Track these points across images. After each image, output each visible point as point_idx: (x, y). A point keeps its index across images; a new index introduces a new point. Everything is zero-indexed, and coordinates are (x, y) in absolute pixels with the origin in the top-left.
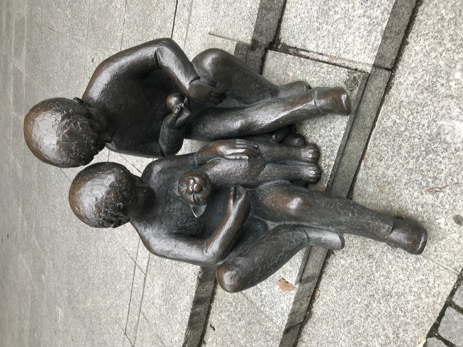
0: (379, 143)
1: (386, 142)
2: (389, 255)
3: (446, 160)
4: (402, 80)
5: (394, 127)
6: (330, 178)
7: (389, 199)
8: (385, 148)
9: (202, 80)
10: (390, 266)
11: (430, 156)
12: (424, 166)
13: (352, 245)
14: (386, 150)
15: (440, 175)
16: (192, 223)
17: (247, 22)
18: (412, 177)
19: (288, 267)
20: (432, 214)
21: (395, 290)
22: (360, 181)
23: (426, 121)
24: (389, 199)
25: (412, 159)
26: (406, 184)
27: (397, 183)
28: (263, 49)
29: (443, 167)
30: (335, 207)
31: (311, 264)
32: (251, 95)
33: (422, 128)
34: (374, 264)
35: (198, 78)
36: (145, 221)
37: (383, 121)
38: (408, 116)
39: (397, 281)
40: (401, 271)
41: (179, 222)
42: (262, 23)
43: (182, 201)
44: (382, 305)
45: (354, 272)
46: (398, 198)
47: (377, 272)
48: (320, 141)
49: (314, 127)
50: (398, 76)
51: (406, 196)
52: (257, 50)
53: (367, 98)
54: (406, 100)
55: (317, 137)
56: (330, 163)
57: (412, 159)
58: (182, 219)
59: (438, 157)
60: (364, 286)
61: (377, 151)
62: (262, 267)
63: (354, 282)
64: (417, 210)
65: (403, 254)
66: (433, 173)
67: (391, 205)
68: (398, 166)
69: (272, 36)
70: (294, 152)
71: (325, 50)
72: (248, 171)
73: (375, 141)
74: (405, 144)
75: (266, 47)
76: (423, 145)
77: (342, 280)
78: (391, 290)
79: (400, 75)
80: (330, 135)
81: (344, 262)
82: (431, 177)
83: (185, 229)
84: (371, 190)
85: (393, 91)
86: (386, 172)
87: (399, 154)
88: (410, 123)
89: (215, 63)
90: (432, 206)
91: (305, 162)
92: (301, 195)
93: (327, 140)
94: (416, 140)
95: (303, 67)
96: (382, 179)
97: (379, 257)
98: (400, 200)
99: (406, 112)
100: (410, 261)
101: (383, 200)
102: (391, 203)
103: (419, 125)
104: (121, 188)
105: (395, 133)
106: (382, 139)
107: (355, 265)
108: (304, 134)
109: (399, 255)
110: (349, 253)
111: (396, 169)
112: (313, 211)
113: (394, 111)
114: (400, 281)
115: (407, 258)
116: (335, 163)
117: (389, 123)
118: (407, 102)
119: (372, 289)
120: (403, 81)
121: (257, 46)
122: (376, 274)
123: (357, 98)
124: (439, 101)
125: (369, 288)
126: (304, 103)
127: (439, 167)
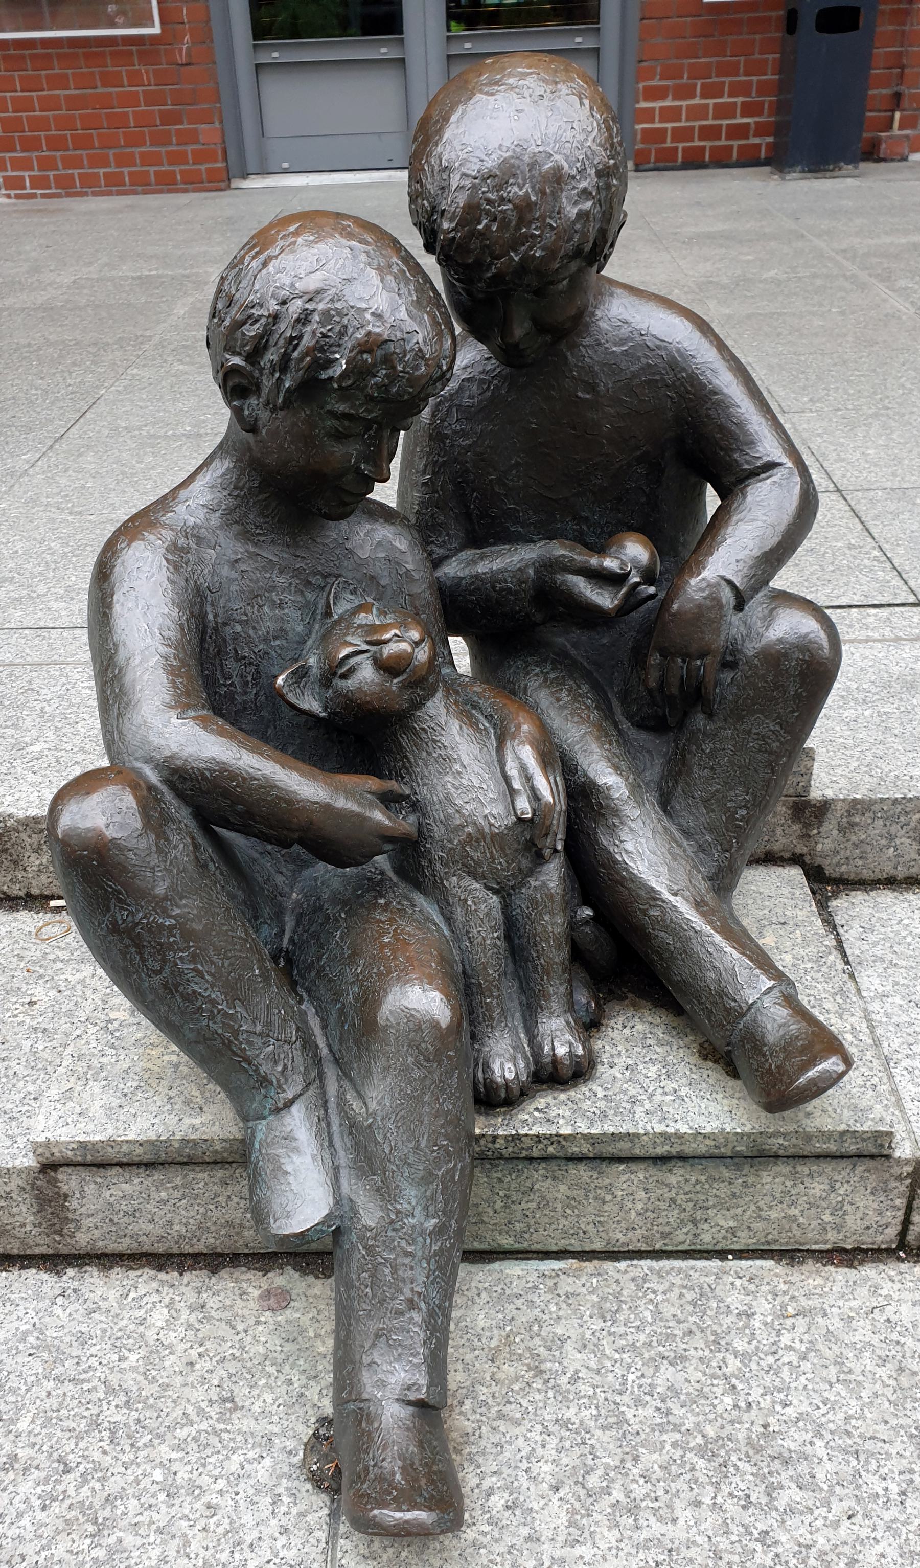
0: (654, 1292)
1: (668, 1311)
2: (267, 1462)
3: (711, 1521)
4: (887, 1288)
5: (731, 1318)
6: (505, 1137)
7: (479, 1387)
8: (647, 1314)
9: (736, 619)
10: (221, 1484)
11: (701, 1463)
12: (655, 1456)
13: (240, 1327)
14: (643, 1321)
15: (653, 1520)
16: (237, 681)
17: (867, 778)
18: (599, 1433)
19: (98, 1104)
20: (501, 1548)
21: (130, 1540)
22: (496, 1276)
23: (805, 1408)
24: (479, 1387)
25: (658, 1409)
26: (565, 1424)
27: (551, 1394)
28: (801, 849)
29: (685, 1515)
30: (448, 1153)
31: (125, 1188)
32: (705, 801)
33: (774, 1402)
34: (204, 1426)
35: (740, 605)
36: (232, 502)
37: (731, 1279)
38: (789, 1348)
39: (174, 1529)
40: (221, 1530)
41: (238, 628)
42: (881, 822)
43: (309, 635)
44: (40, 1516)
45: (134, 1369)
46: (501, 1416)
47: (178, 1448)
48: (615, 1071)
49: (649, 1042)
50: (893, 1273)
51: (521, 1440)
52: (796, 827)
53: (807, 1181)
54: (835, 1324)
55: (621, 1061)
56: (561, 1121)
57: (658, 1409)
58: (249, 642)
59: (710, 1489)
60: (95, 1424)
61: (625, 1293)
62: (171, 928)
63: (95, 1382)
64: (490, 1493)
65: (294, 1511)
66: (647, 1495)
67: (461, 1403)
68: (610, 1377)
69: (844, 868)
70: (556, 988)
71: (884, 1020)
72: (480, 831)
73: (654, 1278)
74: (695, 1369)
75: (807, 859)
76: (722, 1427)
77: (83, 1340)
78: (121, 1524)
79: (896, 1279)
80: (652, 1095)
81: (160, 1324)
82: (628, 1493)
83: (219, 653)
84: (482, 1322)
85: (841, 1275)
86: (569, 1347)
87: (655, 1363)
88: (771, 1359)
89: (804, 646)
90: (529, 1539)
91: (531, 1042)
92: (459, 1025)
93: (632, 1092)
94: (728, 1400)
95: (809, 965)
96: (537, 1341)
97: (239, 1431)
98: (495, 1424)
99: (797, 1336)
100: (279, 1544)
101: (466, 1369)
102: (468, 1402)
103: (780, 1390)
104: (401, 360)
105: (715, 1327)
106: (674, 1296)
107: (167, 1364)
108: (612, 1023)
109: (286, 1500)
110: (205, 1329)
111: (598, 1372)
112: (417, 1073)
113: (779, 1300)
114: (175, 1544)
115: (285, 1531)
116: (566, 1137)
117: (735, 1300)
118: (831, 1328)
119: (97, 1455)
120: (884, 1292)
121: (807, 826)
122: (164, 1448)
123: (808, 1138)
124: (886, 1422)
125: (94, 1446)
126: (751, 961)
127: (678, 1504)
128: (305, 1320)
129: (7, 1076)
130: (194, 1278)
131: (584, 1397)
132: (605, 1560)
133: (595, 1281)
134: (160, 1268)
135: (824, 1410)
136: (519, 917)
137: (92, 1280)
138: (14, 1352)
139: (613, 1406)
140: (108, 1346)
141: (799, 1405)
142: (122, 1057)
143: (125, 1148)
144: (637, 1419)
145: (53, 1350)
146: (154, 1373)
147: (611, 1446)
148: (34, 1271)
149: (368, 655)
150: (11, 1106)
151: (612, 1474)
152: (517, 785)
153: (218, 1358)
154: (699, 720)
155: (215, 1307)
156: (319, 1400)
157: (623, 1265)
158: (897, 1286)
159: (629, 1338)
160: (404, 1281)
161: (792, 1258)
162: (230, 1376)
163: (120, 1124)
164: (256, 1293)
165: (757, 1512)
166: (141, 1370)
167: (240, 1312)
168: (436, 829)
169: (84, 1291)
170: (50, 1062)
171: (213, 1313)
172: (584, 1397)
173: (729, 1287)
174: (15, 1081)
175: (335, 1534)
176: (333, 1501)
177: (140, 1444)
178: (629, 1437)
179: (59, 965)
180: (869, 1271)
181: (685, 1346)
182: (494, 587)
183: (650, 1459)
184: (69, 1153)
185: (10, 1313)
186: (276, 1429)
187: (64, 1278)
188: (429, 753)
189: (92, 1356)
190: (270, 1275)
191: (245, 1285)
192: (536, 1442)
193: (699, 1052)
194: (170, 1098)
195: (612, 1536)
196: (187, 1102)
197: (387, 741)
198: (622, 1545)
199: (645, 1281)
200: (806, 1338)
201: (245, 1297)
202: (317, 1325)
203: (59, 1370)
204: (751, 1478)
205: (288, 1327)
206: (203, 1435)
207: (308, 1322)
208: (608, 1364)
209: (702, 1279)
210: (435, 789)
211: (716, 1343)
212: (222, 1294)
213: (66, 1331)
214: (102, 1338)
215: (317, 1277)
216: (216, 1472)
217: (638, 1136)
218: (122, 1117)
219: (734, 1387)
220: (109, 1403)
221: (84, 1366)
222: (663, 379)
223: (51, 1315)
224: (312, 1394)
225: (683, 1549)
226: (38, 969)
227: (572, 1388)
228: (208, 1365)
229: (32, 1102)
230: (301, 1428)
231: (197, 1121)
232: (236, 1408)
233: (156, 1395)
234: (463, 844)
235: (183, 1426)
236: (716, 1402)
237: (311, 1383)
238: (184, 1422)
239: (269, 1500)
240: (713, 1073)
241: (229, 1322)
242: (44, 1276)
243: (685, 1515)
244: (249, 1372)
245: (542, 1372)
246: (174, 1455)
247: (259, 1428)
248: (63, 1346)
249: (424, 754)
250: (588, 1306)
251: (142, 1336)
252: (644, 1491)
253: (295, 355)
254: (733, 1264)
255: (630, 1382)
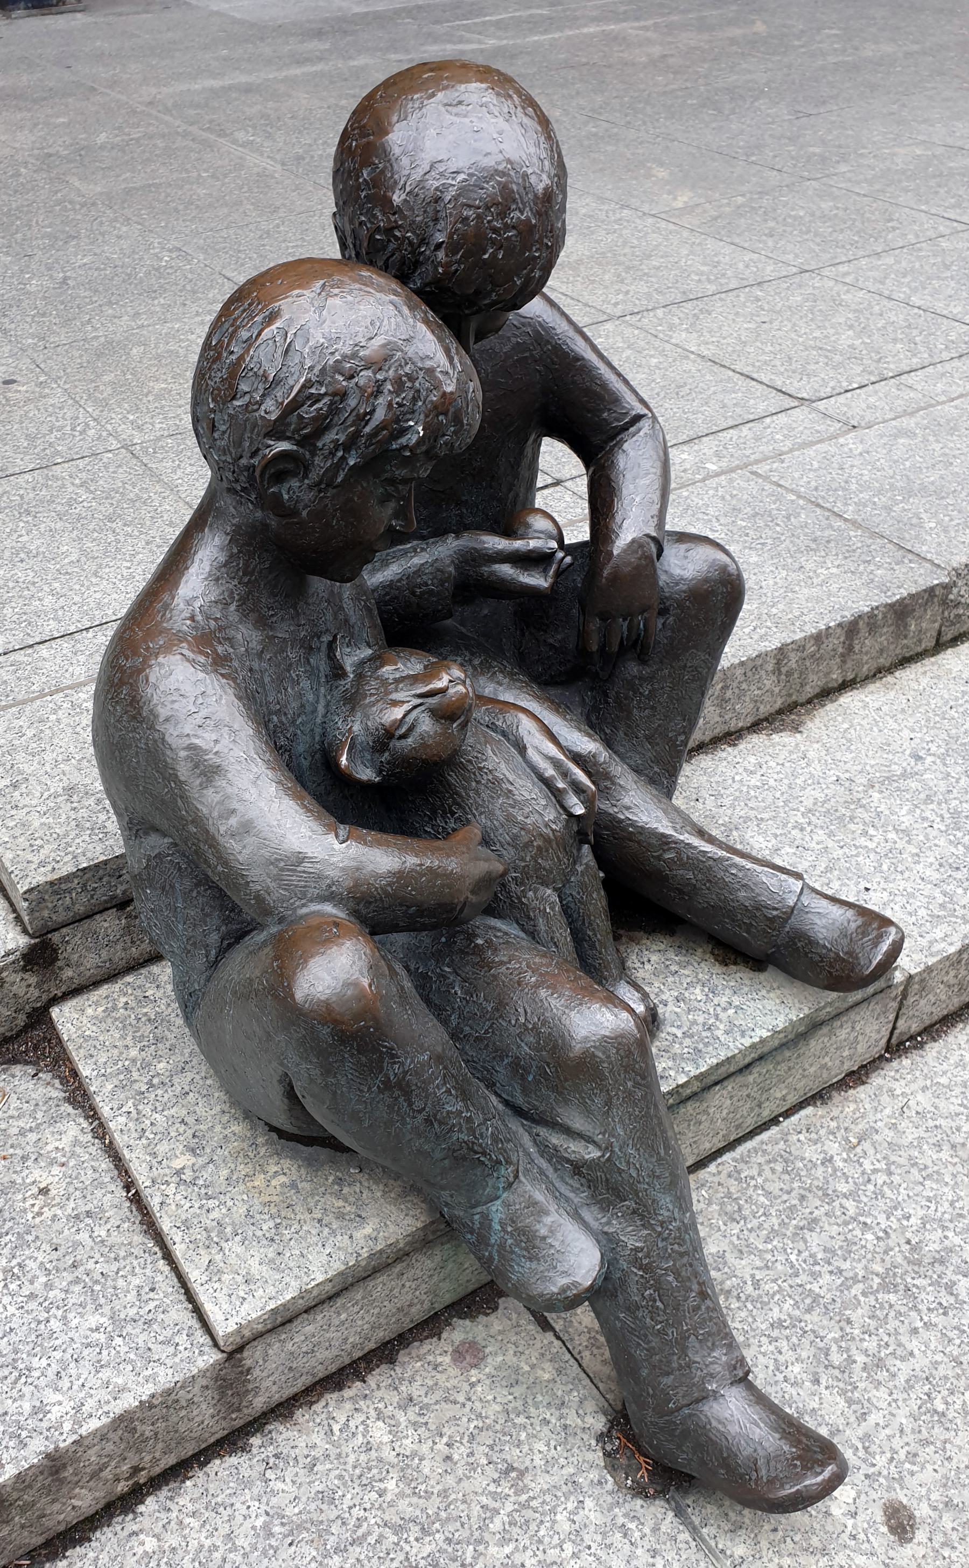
1: (774, 1187)
2: (589, 1503)
3: (933, 1337)
5: (821, 1169)
8: (762, 1199)
11: (892, 1298)
12: (860, 1311)
13: (461, 1398)
18: (807, 1317)
23: (921, 1213)
25: (831, 1272)
26: (779, 1324)
29: (914, 1345)
32: (648, 738)
33: (899, 1220)
34: (509, 1507)
37: (795, 1138)
38: (875, 1171)
45: (401, 1495)
47: (503, 1542)
56: (672, 1073)
63: (377, 1531)
65: (647, 1530)
66: (879, 1346)
72: (547, 840)
77: (327, 1497)
82: (866, 1352)
85: (861, 1092)
88: (871, 1187)
93: (701, 1019)
106: (767, 1173)
107: (426, 1471)
109: (632, 1526)
110: (431, 1418)
115: (654, 1553)
117: (811, 1153)
118: (889, 1139)
122: (493, 1550)
127: (904, 1339)
128: (510, 1358)
129: (97, 1282)
130: (379, 1377)
131: (774, 1294)
132: (894, 1415)
133: (703, 1192)
134: (339, 1387)
135: (933, 1207)
136: (572, 905)
137: (284, 1436)
138: (271, 1552)
139: (800, 1290)
140: (358, 1489)
141: (917, 1214)
142: (230, 1203)
143: (315, 1293)
144: (824, 1289)
145: (309, 1525)
146: (423, 1487)
147: (825, 1322)
148: (217, 1462)
149: (422, 708)
150: (135, 1310)
151: (843, 1344)
152: (561, 785)
153: (466, 1438)
154: (633, 669)
155: (422, 1393)
156: (583, 1422)
157: (712, 1168)
158: (903, 1082)
159: (766, 1226)
160: (689, 1279)
161: (822, 1097)
162: (491, 1447)
163: (296, 1271)
164: (447, 1359)
165: (955, 1312)
166: (408, 1492)
167: (448, 1385)
168: (504, 852)
169: (285, 1451)
170: (130, 1244)
171: (426, 1401)
172: (774, 1294)
173: (798, 1144)
174: (110, 1283)
175: (694, 1528)
176: (668, 1501)
177: (469, 1560)
178: (831, 1307)
179: (32, 1137)
180: (876, 1080)
181: (808, 1210)
182: (413, 593)
183: (857, 1315)
184: (260, 1326)
185: (231, 1518)
186: (572, 1470)
187: (254, 1451)
188: (478, 782)
189: (350, 1508)
190: (444, 1335)
191: (430, 1358)
192: (772, 1353)
193: (716, 960)
194: (320, 1221)
195: (883, 1393)
196: (340, 1216)
197: (432, 783)
198: (895, 1396)
199: (739, 1172)
200: (878, 1156)
201: (440, 1369)
202: (523, 1357)
203: (332, 1542)
204: (931, 1288)
205: (502, 1374)
206: (516, 1515)
207: (515, 1359)
208: (769, 1256)
209: (776, 1148)
210: (494, 815)
211: (827, 1196)
212: (418, 1378)
213: (304, 1499)
214: (345, 1484)
215: (487, 1315)
216: (556, 1540)
217: (734, 1057)
218: (291, 1264)
219: (865, 1224)
220: (406, 1541)
221: (352, 1522)
222: (532, 355)
223: (274, 1493)
224: (572, 1419)
225: (934, 1372)
226: (11, 1151)
227: (761, 1292)
228: (464, 1450)
229: (151, 1295)
230: (590, 1456)
231: (368, 1230)
232: (522, 1474)
233: (443, 1506)
234: (534, 858)
235: (491, 1518)
236: (863, 1242)
237: (565, 1411)
238: (488, 1514)
239: (618, 1535)
240: (742, 975)
241: (446, 1400)
242: (233, 1460)
243: (914, 1345)
244: (504, 1435)
245: (729, 1292)
246: (508, 1550)
247: (556, 1478)
248: (315, 1516)
249: (474, 784)
250: (716, 1216)
251: (380, 1460)
252: (875, 1344)
253: (368, 429)
254: (786, 1124)
255: (795, 1262)
